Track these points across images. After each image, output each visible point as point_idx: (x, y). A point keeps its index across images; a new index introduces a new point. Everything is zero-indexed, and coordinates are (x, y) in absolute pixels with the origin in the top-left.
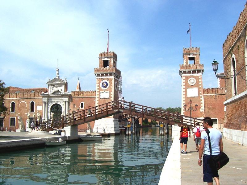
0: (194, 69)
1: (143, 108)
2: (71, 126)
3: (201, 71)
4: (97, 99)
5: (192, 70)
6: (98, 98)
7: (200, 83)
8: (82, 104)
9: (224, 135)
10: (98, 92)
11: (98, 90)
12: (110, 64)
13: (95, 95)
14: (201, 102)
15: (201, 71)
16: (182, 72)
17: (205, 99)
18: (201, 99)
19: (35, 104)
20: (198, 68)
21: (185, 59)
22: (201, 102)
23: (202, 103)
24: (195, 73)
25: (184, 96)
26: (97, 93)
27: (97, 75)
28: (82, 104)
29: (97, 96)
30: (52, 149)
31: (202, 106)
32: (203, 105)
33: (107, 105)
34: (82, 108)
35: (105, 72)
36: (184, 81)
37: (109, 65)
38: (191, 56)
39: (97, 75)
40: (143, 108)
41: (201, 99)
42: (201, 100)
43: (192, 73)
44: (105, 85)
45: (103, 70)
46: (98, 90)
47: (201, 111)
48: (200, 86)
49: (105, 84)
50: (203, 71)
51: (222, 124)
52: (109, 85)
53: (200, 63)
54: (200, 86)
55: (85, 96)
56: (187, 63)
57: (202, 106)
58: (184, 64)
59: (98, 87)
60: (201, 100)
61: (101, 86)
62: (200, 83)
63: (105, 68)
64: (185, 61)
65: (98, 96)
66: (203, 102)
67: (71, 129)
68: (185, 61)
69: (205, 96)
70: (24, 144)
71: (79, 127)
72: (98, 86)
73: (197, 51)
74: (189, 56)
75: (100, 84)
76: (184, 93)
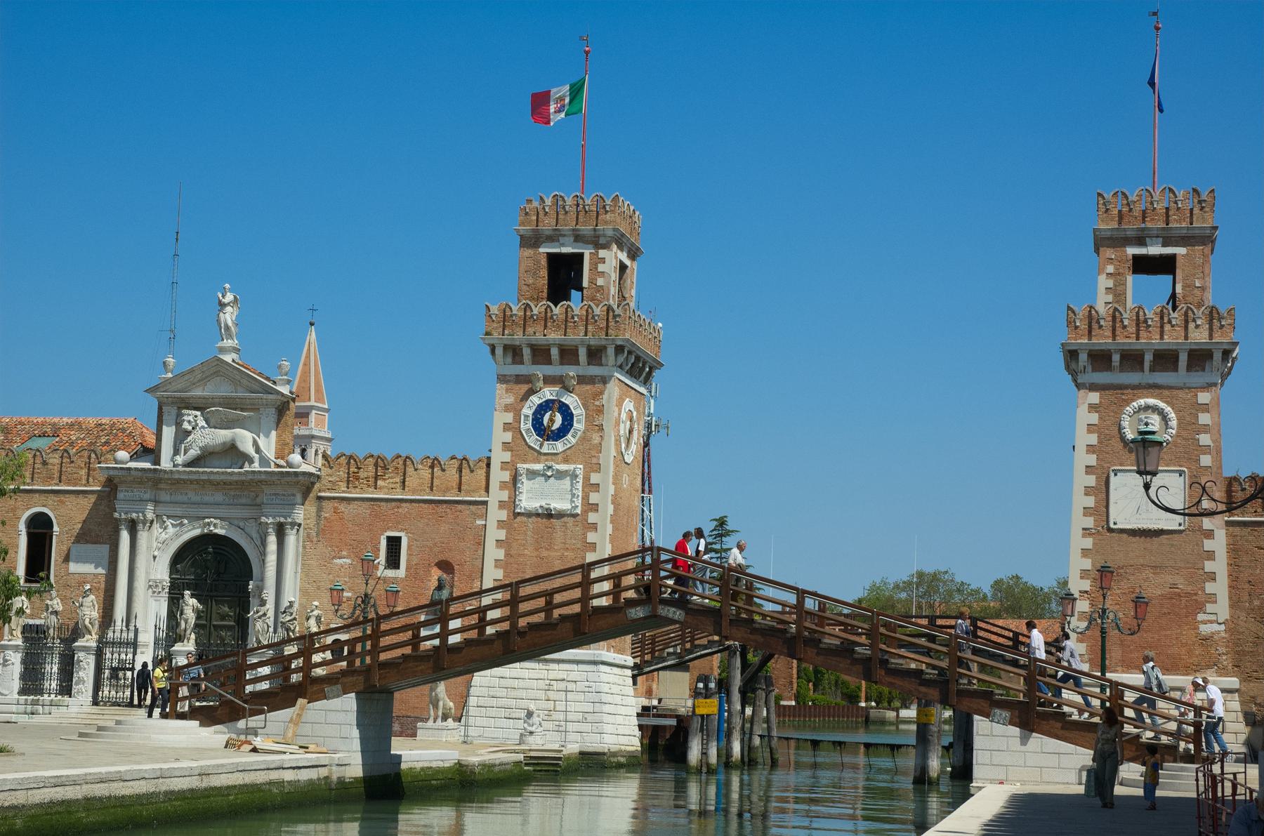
0: (1172, 338)
1: (801, 602)
2: (357, 693)
3: (1218, 356)
4: (496, 514)
5: (1151, 340)
6: (502, 505)
7: (1205, 439)
8: (394, 544)
9: (732, 551)
10: (504, 466)
11: (507, 456)
12: (592, 282)
13: (487, 489)
14: (1209, 566)
15: (1218, 356)
16: (1083, 357)
17: (1234, 550)
18: (1208, 545)
19: (56, 528)
20: (1199, 336)
21: (1110, 269)
22: (1209, 566)
23: (1212, 577)
24: (1176, 369)
25: (1089, 522)
26: (499, 476)
27: (499, 351)
28: (394, 544)
29: (497, 495)
30: (496, 808)
31: (1212, 598)
32: (1220, 588)
33: (586, 576)
34: (390, 573)
35: (554, 336)
36: (1094, 418)
37: (585, 284)
38: (1155, 250)
39: (499, 351)
40: (801, 602)
41: (1208, 545)
42: (1211, 555)
43: (1152, 370)
44: (552, 420)
45: (546, 319)
46: (507, 456)
47: (1205, 629)
48: (1206, 460)
49: (559, 420)
50: (1226, 354)
51: (288, 793)
52: (578, 425)
53: (1210, 299)
54: (1206, 460)
55: (414, 492)
56: (1118, 293)
57: (1212, 598)
58: (1102, 303)
59: (508, 437)
60: (1211, 555)
61: (526, 425)
62: (1205, 439)
63: (557, 310)
64: (1110, 284)
65: (505, 495)
66: (1219, 566)
67: (361, 712)
68: (1104, 282)
69: (1237, 530)
70: (212, 784)
71: (405, 699)
72: (507, 427)
73: (1196, 211)
74: (1132, 251)
75: (517, 419)
76: (1090, 502)
